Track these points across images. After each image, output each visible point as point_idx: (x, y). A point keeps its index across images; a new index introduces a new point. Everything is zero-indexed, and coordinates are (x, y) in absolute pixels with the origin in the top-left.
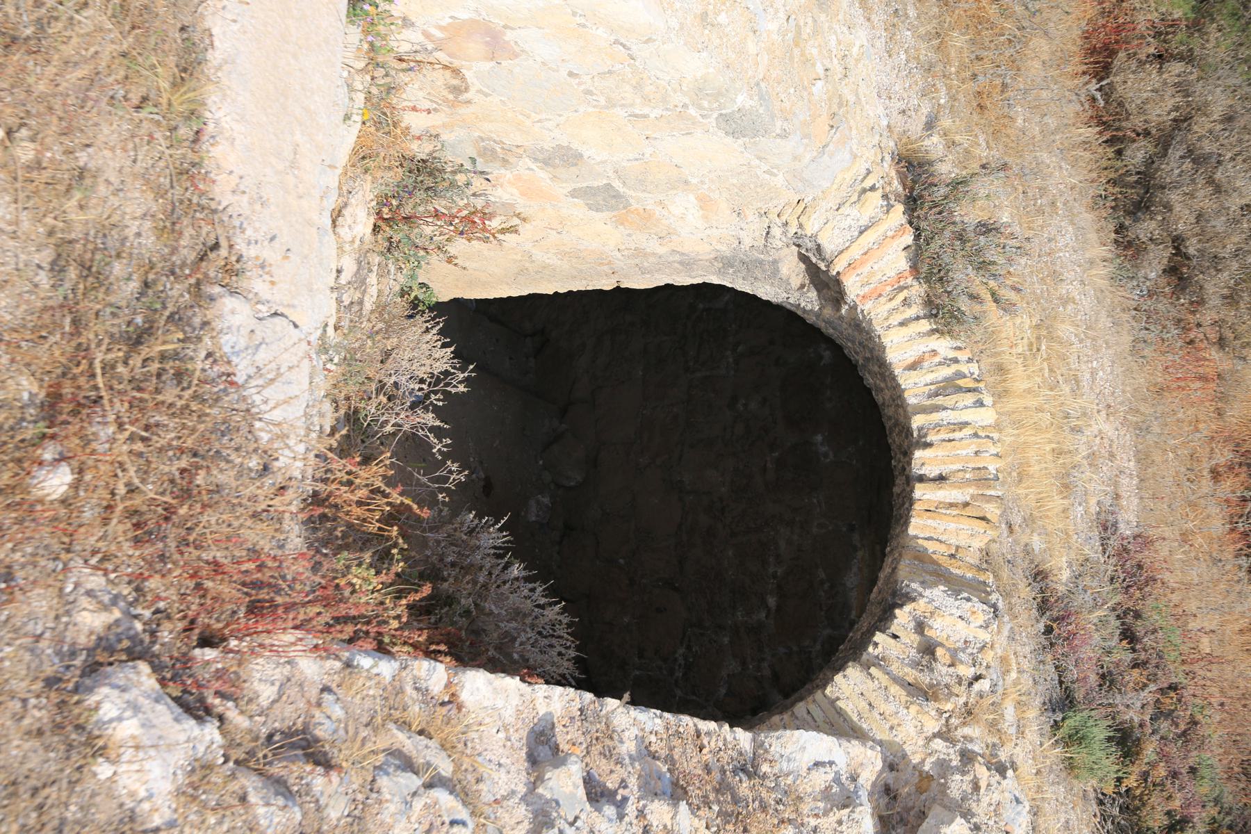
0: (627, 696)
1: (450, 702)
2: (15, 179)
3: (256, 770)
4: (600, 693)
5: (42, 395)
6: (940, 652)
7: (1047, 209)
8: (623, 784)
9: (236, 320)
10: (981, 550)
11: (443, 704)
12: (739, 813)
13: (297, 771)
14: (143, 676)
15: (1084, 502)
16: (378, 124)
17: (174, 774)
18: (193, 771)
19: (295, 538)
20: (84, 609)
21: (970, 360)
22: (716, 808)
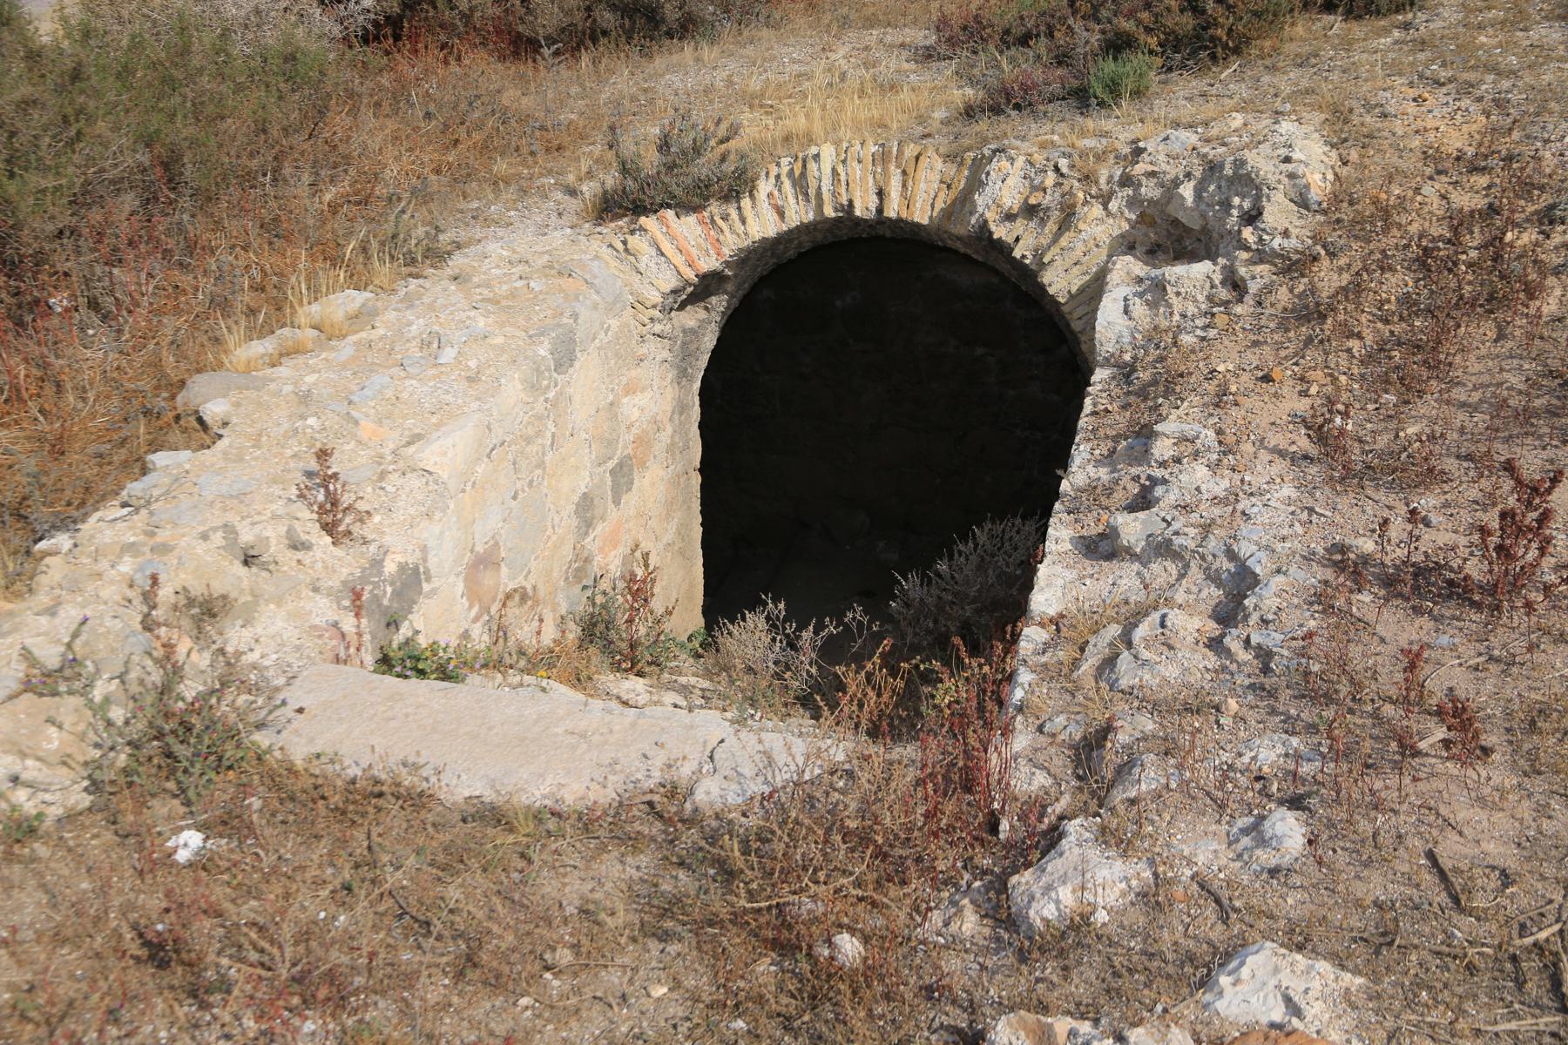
0: (1060, 472)
1: (1057, 624)
2: (587, 965)
3: (1108, 791)
4: (1055, 495)
5: (773, 955)
6: (1032, 201)
7: (650, 95)
8: (1136, 479)
9: (715, 791)
10: (945, 162)
11: (1058, 630)
12: (1166, 380)
13: (1111, 756)
14: (1023, 881)
15: (906, 74)
16: (551, 666)
17: (1108, 858)
18: (1105, 842)
19: (909, 751)
20: (960, 928)
21: (778, 165)
22: (1160, 400)
